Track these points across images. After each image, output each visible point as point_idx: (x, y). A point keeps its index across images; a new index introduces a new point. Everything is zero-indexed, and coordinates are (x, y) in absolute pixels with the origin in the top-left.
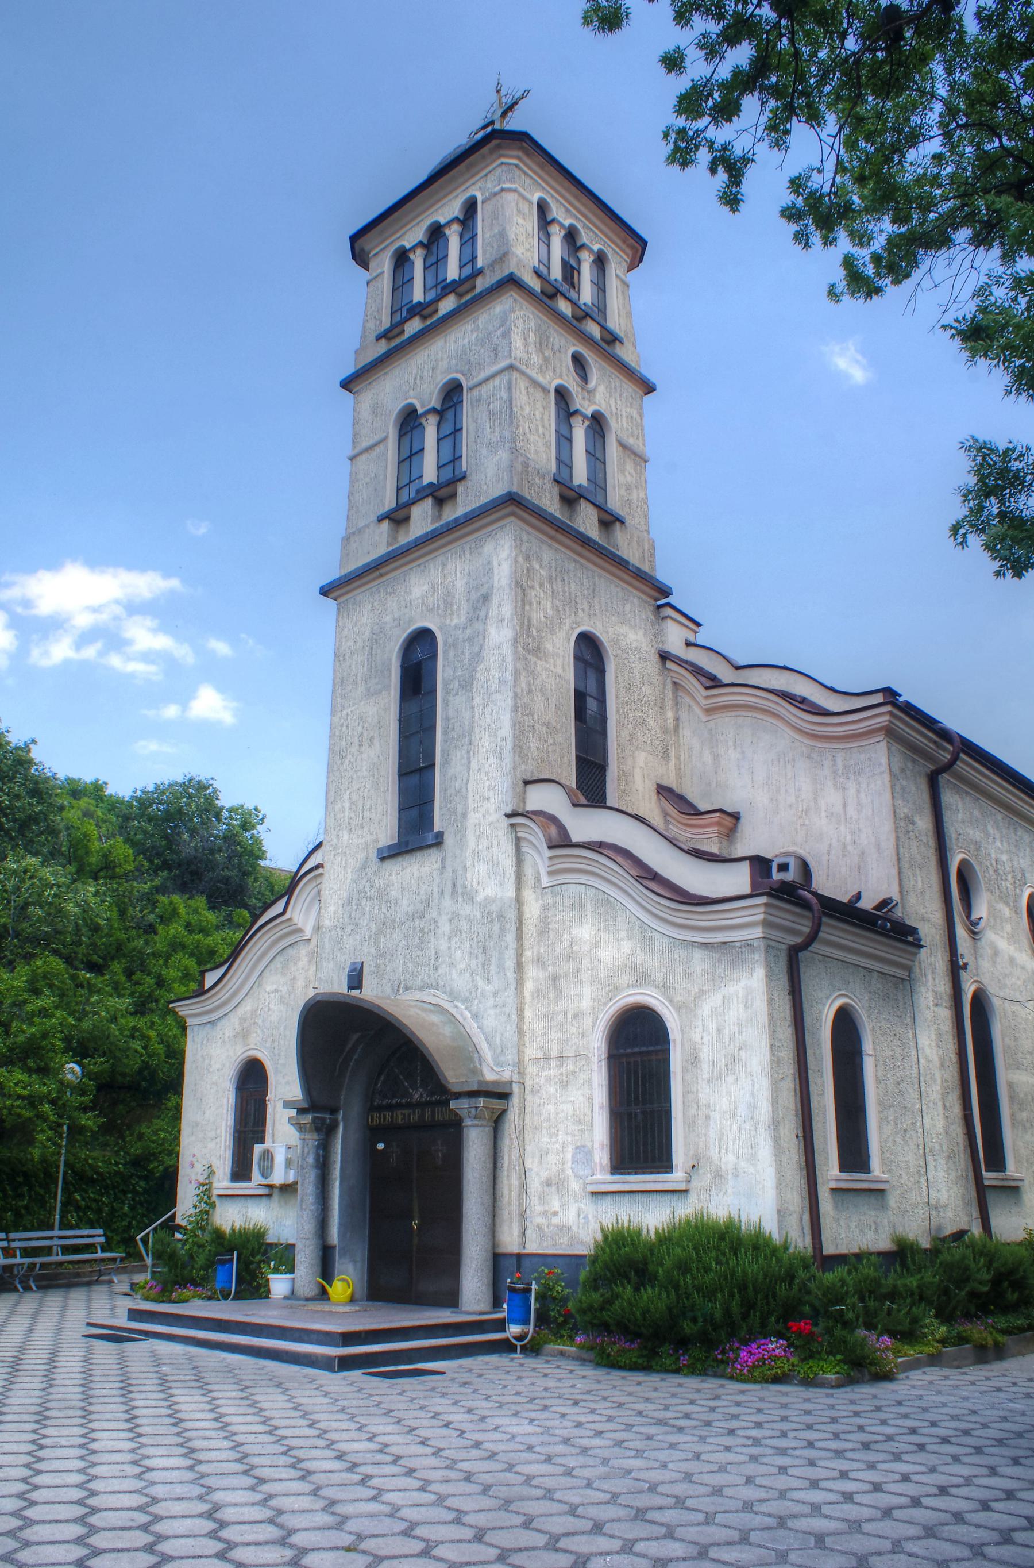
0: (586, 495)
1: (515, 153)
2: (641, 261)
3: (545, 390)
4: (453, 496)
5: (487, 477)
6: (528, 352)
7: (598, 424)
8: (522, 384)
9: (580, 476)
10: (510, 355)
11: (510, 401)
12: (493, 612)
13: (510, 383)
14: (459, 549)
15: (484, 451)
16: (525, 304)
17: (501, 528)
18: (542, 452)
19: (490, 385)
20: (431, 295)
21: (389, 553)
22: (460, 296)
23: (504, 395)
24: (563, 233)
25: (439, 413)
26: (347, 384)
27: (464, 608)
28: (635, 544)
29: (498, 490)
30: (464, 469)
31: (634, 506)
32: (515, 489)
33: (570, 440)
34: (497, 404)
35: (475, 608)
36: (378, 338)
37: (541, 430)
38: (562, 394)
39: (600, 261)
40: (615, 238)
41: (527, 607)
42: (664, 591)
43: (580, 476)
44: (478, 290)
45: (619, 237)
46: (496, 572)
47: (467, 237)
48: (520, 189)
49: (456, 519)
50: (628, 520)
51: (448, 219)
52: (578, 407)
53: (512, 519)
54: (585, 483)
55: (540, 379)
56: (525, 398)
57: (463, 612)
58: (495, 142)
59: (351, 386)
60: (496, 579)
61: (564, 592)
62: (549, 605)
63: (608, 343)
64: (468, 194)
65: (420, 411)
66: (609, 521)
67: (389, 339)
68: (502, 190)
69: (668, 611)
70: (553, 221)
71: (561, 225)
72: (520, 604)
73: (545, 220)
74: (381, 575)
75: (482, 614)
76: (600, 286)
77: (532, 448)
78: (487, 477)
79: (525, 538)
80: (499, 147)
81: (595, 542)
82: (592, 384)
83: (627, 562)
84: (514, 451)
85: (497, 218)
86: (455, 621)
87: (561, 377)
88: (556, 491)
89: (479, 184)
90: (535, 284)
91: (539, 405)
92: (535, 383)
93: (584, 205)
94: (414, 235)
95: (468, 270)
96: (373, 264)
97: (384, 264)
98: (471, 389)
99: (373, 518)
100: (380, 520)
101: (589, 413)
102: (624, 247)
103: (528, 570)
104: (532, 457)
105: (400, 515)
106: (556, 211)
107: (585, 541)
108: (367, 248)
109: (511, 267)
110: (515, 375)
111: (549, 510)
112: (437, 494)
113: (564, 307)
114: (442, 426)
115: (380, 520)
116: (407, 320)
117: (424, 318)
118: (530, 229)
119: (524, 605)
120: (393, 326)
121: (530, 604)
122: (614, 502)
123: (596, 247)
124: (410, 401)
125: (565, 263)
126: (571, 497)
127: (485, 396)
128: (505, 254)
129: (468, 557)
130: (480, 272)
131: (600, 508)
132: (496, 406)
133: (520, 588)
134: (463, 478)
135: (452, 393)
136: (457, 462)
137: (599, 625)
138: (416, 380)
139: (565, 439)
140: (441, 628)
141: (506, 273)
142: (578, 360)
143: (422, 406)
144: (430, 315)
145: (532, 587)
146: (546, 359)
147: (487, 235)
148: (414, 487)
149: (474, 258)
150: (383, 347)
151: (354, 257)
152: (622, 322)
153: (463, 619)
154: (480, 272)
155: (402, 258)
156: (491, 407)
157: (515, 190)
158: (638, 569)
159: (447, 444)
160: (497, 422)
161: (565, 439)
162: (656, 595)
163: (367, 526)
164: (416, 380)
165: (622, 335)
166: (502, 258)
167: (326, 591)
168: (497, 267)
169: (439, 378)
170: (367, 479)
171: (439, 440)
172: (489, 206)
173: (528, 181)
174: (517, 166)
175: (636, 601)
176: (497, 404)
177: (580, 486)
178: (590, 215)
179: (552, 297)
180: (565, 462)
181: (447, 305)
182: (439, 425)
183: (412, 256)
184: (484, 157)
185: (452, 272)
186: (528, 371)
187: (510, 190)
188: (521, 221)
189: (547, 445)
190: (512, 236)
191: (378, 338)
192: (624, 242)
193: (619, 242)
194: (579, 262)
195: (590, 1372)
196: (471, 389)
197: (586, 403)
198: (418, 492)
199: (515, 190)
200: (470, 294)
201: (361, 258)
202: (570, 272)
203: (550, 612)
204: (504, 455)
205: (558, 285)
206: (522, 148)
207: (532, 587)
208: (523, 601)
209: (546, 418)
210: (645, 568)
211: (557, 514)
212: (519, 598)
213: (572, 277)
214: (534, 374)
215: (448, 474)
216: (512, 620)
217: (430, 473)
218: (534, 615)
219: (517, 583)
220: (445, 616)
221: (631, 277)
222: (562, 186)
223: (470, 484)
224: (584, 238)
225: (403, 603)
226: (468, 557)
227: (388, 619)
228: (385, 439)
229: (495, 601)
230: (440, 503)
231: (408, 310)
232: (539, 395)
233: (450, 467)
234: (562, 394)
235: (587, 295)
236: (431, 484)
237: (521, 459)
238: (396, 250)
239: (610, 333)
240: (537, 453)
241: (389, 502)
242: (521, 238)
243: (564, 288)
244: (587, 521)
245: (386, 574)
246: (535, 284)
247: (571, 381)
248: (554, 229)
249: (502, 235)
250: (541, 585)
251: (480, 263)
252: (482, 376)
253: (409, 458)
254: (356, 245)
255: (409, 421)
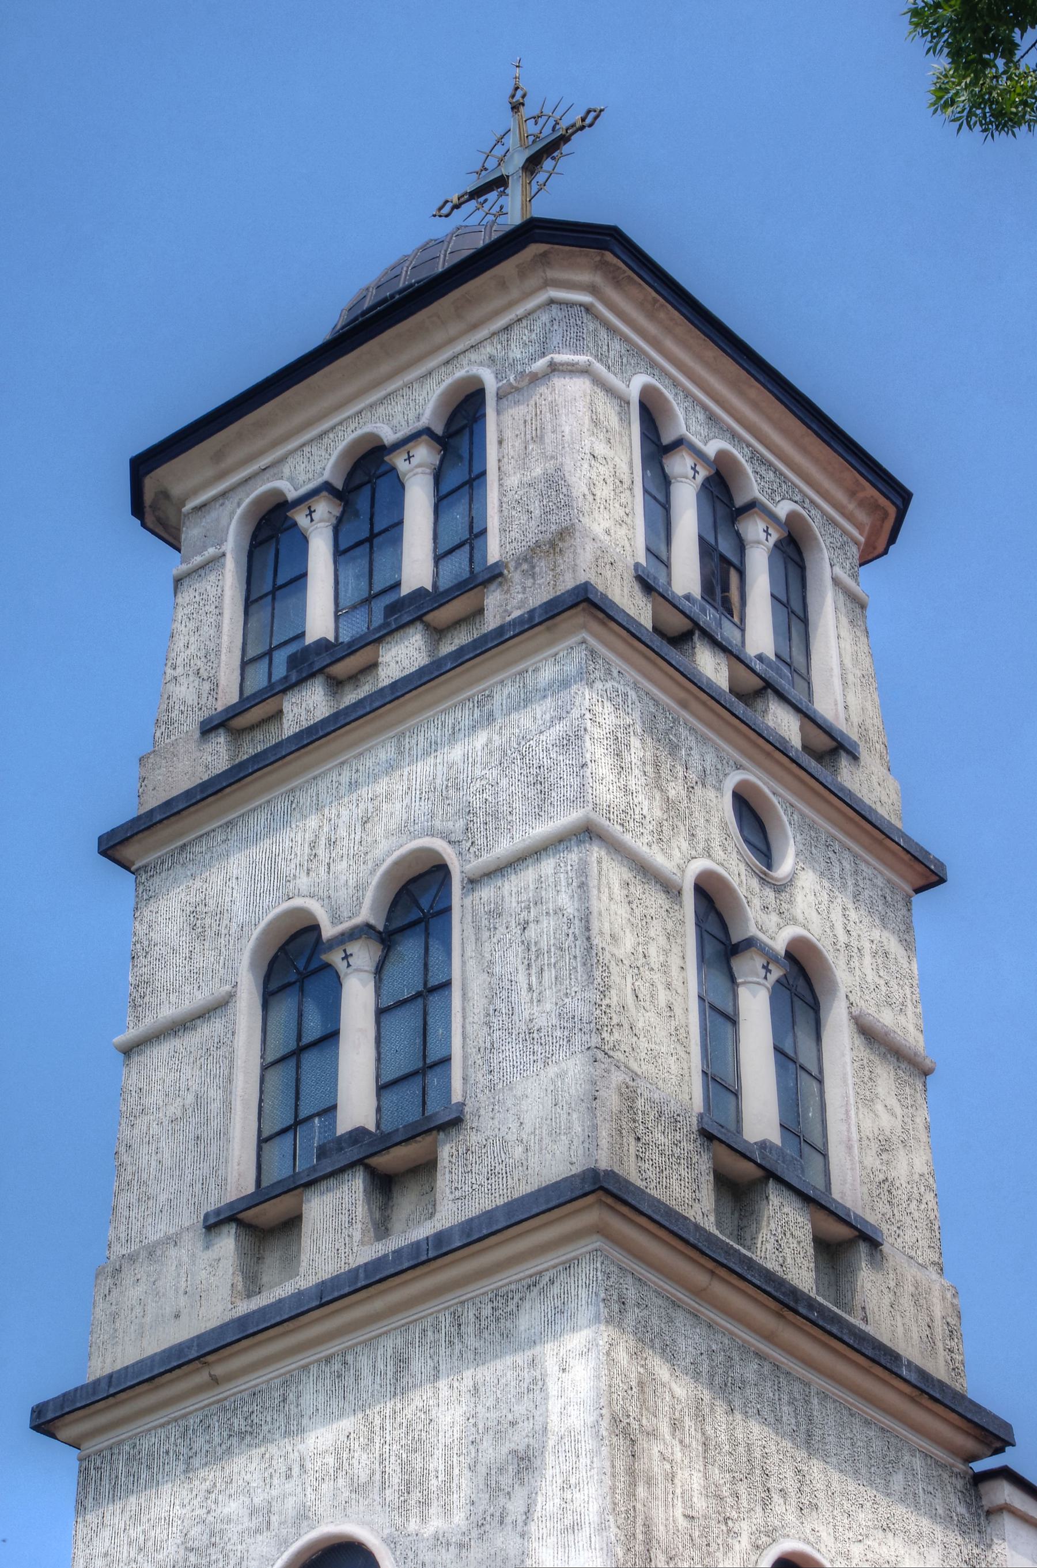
0: (781, 1170)
1: (585, 277)
2: (892, 539)
3: (670, 889)
4: (427, 1167)
5: (524, 1116)
6: (626, 790)
7: (801, 983)
8: (614, 874)
9: (760, 1119)
10: (580, 797)
11: (586, 920)
12: (549, 1499)
13: (583, 870)
14: (446, 1321)
15: (511, 1052)
16: (618, 663)
17: (568, 1266)
18: (671, 1066)
19: (528, 875)
20: (355, 627)
21: (242, 1321)
22: (437, 633)
23: (566, 900)
24: (703, 473)
25: (386, 938)
26: (114, 846)
27: (465, 1486)
28: (906, 1302)
29: (553, 1162)
30: (456, 1097)
31: (901, 1195)
32: (604, 1164)
33: (733, 1020)
34: (548, 924)
35: (494, 1490)
36: (208, 729)
37: (663, 996)
38: (711, 901)
39: (793, 550)
40: (827, 484)
41: (641, 1491)
42: (994, 1437)
43: (760, 1119)
44: (491, 621)
45: (839, 482)
46: (553, 1388)
47: (455, 477)
48: (599, 368)
49: (440, 1238)
50: (887, 1234)
51: (404, 432)
52: (753, 931)
53: (596, 1242)
54: (774, 1136)
55: (659, 859)
56: (623, 911)
57: (459, 1499)
58: (534, 249)
59: (128, 852)
60: (554, 1406)
61: (734, 1443)
62: (697, 1482)
63: (820, 757)
64: (460, 373)
65: (328, 931)
66: (845, 1241)
67: (237, 734)
68: (554, 368)
69: (1006, 1493)
70: (679, 443)
71: (699, 454)
72: (622, 1480)
73: (658, 447)
74: (215, 1381)
75: (516, 1507)
76: (794, 613)
77: (643, 1043)
78: (524, 1116)
79: (631, 1293)
80: (543, 260)
81: (811, 1304)
82: (785, 867)
83: (896, 1357)
84: (600, 1054)
85: (539, 438)
86: (436, 1524)
87: (708, 853)
88: (704, 1164)
89: (488, 349)
90: (639, 609)
91: (656, 929)
92: (644, 871)
93: (755, 405)
94: (306, 462)
95: (457, 567)
96: (191, 534)
97: (224, 534)
98: (473, 882)
99: (190, 1218)
100: (213, 1225)
101: (779, 945)
102: (851, 506)
103: (641, 1384)
104: (644, 1068)
105: (273, 1211)
106: (684, 421)
107: (784, 1299)
108: (177, 490)
109: (580, 567)
110: (596, 852)
111: (690, 1214)
112: (374, 1161)
113: (710, 666)
114: (389, 969)
115: (213, 1225)
116: (288, 686)
117: (336, 685)
118: (623, 467)
119: (633, 1484)
120: (246, 703)
121: (649, 1482)
122: (849, 1184)
123: (783, 509)
124: (297, 902)
125: (707, 549)
126: (743, 1180)
127: (512, 904)
128: (565, 533)
129: (472, 1341)
130: (495, 575)
131: (815, 1202)
132: (545, 931)
133: (625, 1434)
134: (455, 1123)
135: (418, 902)
136: (433, 1079)
137: (825, 1533)
138: (326, 848)
139: (720, 1018)
140: (391, 1542)
141: (568, 583)
142: (748, 810)
143: (335, 919)
144: (354, 678)
145: (653, 1434)
146: (669, 804)
147: (513, 481)
148: (315, 1133)
149: (476, 535)
150: (217, 756)
151: (138, 509)
152: (852, 700)
153: (459, 1518)
154: (495, 575)
155: (273, 530)
156: (532, 932)
157: (585, 371)
158: (923, 1374)
159: (405, 1022)
160: (549, 975)
161: (720, 1018)
162: (969, 1444)
163: (173, 1240)
164: (326, 848)
165: (853, 735)
166: (557, 541)
167: (47, 1421)
168: (542, 565)
169: (383, 846)
170: (174, 1109)
171: (381, 1012)
172: (517, 412)
173: (617, 346)
174: (588, 309)
175: (918, 1463)
176: (548, 924)
177: (763, 1145)
178: (767, 428)
179: (681, 640)
180: (722, 1083)
181: (404, 655)
182: (379, 971)
183: (301, 519)
184: (503, 285)
185: (416, 566)
186: (627, 838)
187: (573, 370)
188: (601, 449)
189: (678, 1036)
190: (579, 487)
191: (208, 729)
192: (852, 494)
193: (841, 496)
194: (741, 546)
195: (306, 1241)
196: (473, 882)
197: (772, 920)
198: (323, 1152)
199: (585, 371)
200: (470, 630)
201: (153, 511)
202: (722, 571)
203: (700, 1504)
204: (572, 1069)
205: (695, 610)
206: (602, 266)
207: (653, 1434)
208: (631, 1473)
209: (675, 962)
210: (939, 1369)
211: (710, 1224)
212: (620, 1465)
213: (726, 588)
214: (641, 844)
215: (405, 1107)
216: (602, 1527)
217: (357, 1104)
218: (659, 1514)
219: (615, 1420)
220: (403, 1509)
221: (871, 580)
222: (700, 358)
223: (474, 1139)
224: (754, 485)
225: (280, 1466)
226: (472, 1341)
227: (232, 1507)
228: (220, 1006)
229: (553, 1469)
230: (384, 1186)
231: (294, 662)
232: (655, 900)
233: (412, 1090)
234: (711, 901)
235: (760, 634)
236: (358, 1135)
237: (617, 1077)
238: (258, 502)
239: (826, 730)
240: (654, 1058)
241: (238, 1177)
242: (604, 492)
243: (709, 617)
244: (782, 1238)
245: (230, 1377)
246: (639, 609)
247: (733, 866)
248: (680, 465)
249: (555, 483)
250: (675, 1426)
251: (494, 551)
252: (504, 847)
253: (301, 1053)
254: (150, 484)
255: (296, 962)
